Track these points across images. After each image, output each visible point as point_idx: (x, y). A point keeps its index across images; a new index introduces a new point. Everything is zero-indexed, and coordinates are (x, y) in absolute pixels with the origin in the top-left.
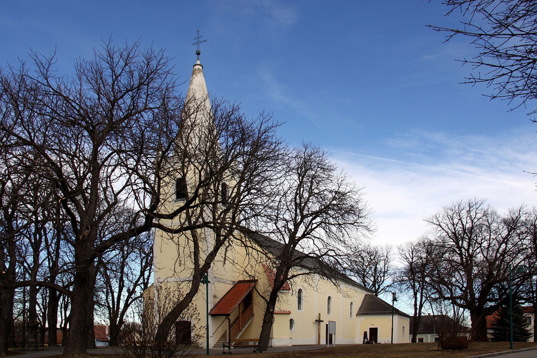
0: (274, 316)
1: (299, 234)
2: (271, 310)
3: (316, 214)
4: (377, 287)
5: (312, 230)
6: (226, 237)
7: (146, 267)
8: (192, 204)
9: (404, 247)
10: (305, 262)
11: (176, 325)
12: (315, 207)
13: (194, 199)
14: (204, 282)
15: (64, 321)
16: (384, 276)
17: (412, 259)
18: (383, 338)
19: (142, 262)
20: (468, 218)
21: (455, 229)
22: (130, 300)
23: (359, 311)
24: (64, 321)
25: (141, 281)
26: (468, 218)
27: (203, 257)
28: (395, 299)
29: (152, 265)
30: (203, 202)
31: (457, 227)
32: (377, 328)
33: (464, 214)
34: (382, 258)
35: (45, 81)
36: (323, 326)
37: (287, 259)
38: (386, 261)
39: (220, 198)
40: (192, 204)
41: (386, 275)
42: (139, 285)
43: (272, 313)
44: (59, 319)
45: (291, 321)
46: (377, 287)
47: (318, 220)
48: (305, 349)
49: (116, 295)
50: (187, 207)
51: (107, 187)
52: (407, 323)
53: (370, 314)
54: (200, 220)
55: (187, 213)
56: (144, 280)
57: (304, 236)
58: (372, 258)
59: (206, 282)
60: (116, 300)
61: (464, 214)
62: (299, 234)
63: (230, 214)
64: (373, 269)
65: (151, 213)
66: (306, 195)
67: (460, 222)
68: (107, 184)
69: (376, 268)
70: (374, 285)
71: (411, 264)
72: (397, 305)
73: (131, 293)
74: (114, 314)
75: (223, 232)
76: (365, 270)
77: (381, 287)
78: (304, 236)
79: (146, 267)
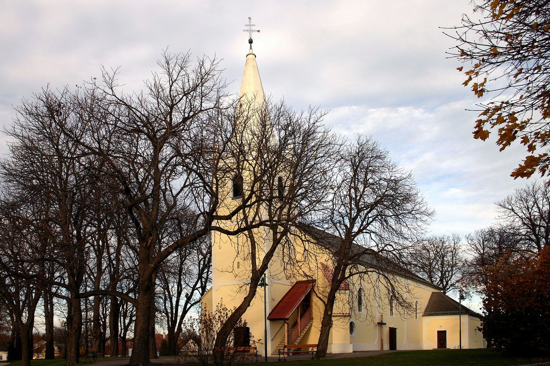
0: (333, 319)
1: (355, 229)
2: (329, 313)
3: (372, 207)
4: (445, 283)
5: (368, 224)
6: (284, 234)
7: (203, 269)
8: (249, 203)
9: (473, 235)
10: (367, 258)
11: (235, 326)
12: (370, 199)
13: (250, 197)
14: (262, 285)
15: (123, 331)
16: (452, 270)
17: (483, 250)
18: (452, 344)
19: (199, 263)
20: (545, 200)
21: (530, 214)
22: (189, 305)
23: (425, 311)
24: (123, 331)
25: (199, 285)
26: (545, 200)
27: (261, 256)
28: (462, 298)
29: (209, 267)
30: (259, 200)
31: (533, 211)
32: (438, 332)
33: (539, 195)
34: (450, 249)
35: (110, 92)
36: (386, 330)
37: (347, 254)
38: (454, 253)
39: (276, 194)
40: (249, 203)
41: (454, 269)
42: (197, 289)
43: (331, 316)
44: (120, 328)
45: (352, 325)
46: (445, 283)
47: (374, 212)
48: (367, 355)
49: (174, 300)
50: (243, 207)
51: (166, 189)
52: (478, 323)
53: (438, 315)
54: (257, 218)
55: (244, 212)
56: (202, 284)
57: (360, 231)
58: (439, 250)
59: (264, 284)
60: (174, 305)
61: (539, 195)
62: (355, 229)
63: (285, 210)
64: (440, 262)
65: (211, 216)
66: (361, 187)
67: (535, 205)
68: (166, 187)
69: (442, 262)
70: (441, 281)
71: (481, 254)
72: (464, 303)
73: (189, 298)
74: (172, 323)
75: (280, 228)
76: (431, 264)
77: (449, 283)
78: (360, 231)
79: (203, 269)
